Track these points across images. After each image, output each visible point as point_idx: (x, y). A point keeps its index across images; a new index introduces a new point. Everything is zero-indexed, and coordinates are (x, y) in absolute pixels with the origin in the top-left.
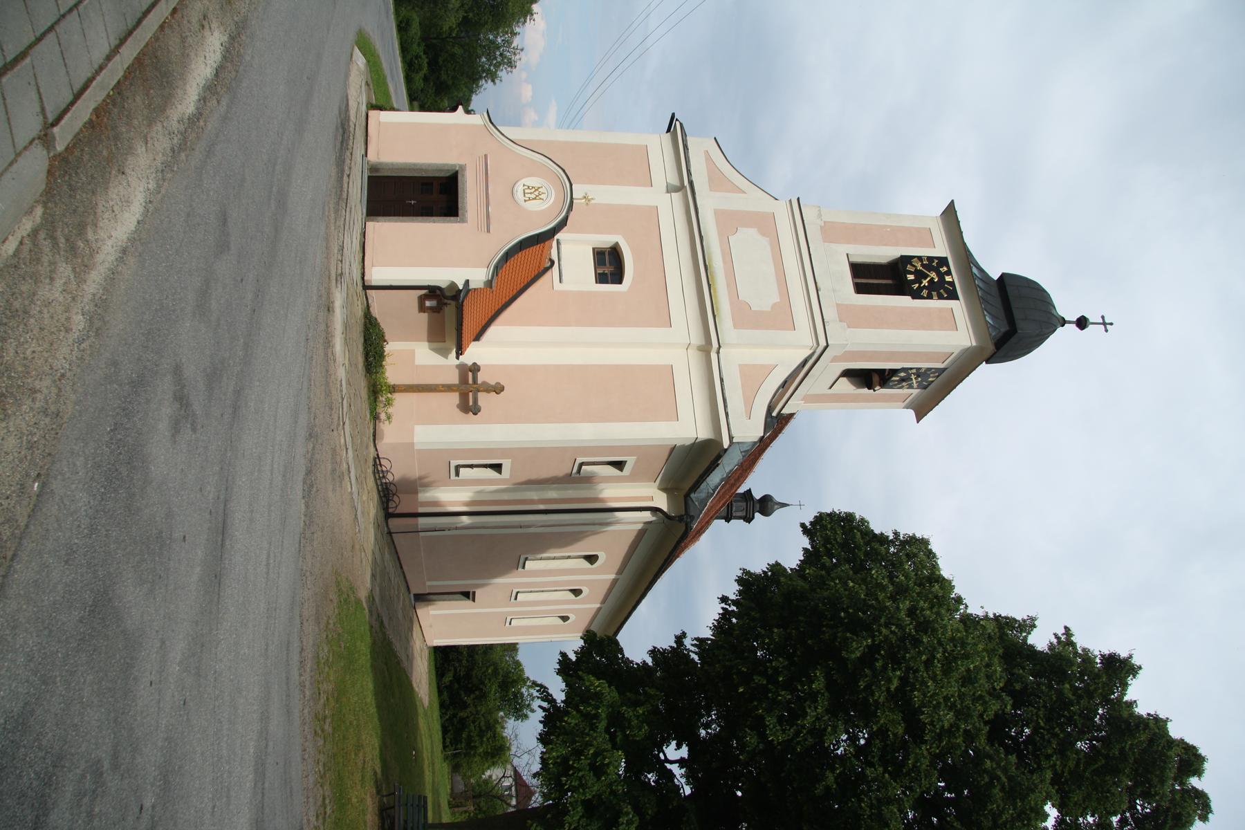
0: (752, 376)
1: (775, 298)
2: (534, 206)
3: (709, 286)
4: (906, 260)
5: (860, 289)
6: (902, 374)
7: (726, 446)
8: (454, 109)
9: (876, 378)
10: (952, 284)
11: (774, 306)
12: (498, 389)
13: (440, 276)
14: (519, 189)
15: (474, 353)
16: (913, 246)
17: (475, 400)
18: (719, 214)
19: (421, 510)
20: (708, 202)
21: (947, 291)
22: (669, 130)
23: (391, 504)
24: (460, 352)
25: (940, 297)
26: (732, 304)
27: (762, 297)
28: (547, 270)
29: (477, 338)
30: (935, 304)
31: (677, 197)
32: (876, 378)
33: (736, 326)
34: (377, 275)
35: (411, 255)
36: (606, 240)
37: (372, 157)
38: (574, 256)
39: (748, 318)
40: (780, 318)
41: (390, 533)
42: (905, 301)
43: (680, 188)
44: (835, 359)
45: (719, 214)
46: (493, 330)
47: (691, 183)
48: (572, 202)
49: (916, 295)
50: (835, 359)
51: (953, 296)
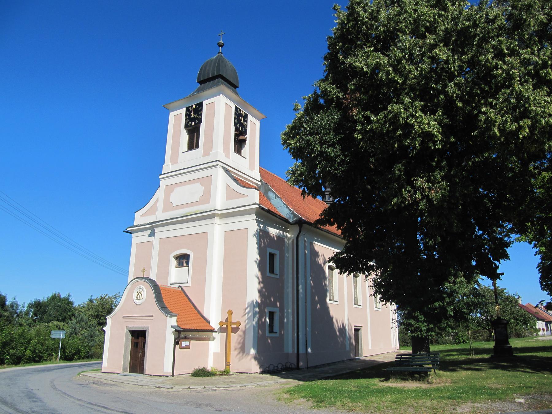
0: (230, 194)
1: (199, 184)
2: (145, 295)
3: (191, 215)
4: (186, 126)
5: (197, 147)
6: (238, 125)
7: (258, 206)
8: (104, 332)
9: (241, 138)
10: (196, 105)
11: (202, 185)
12: (230, 313)
13: (171, 338)
14: (137, 302)
15: (214, 324)
16: (181, 123)
17: (234, 324)
18: (165, 210)
19: (296, 352)
20: (161, 215)
21: (199, 107)
22: (131, 233)
23: (293, 366)
24: (213, 331)
25: (201, 110)
26: (200, 204)
27: (198, 190)
28: (182, 289)
29: (209, 322)
30: (204, 112)
31: (156, 230)
32: (241, 138)
33: (209, 202)
34: (168, 370)
35: (162, 352)
36: (173, 262)
37: (120, 371)
38: (175, 276)
39: (206, 197)
40: (207, 182)
41: (308, 368)
42: (202, 126)
43: (153, 229)
44: (228, 156)
45: (165, 210)
46: (205, 315)
47: (151, 223)
48: (137, 278)
49: (200, 121)
50: (228, 156)
51: (201, 105)
